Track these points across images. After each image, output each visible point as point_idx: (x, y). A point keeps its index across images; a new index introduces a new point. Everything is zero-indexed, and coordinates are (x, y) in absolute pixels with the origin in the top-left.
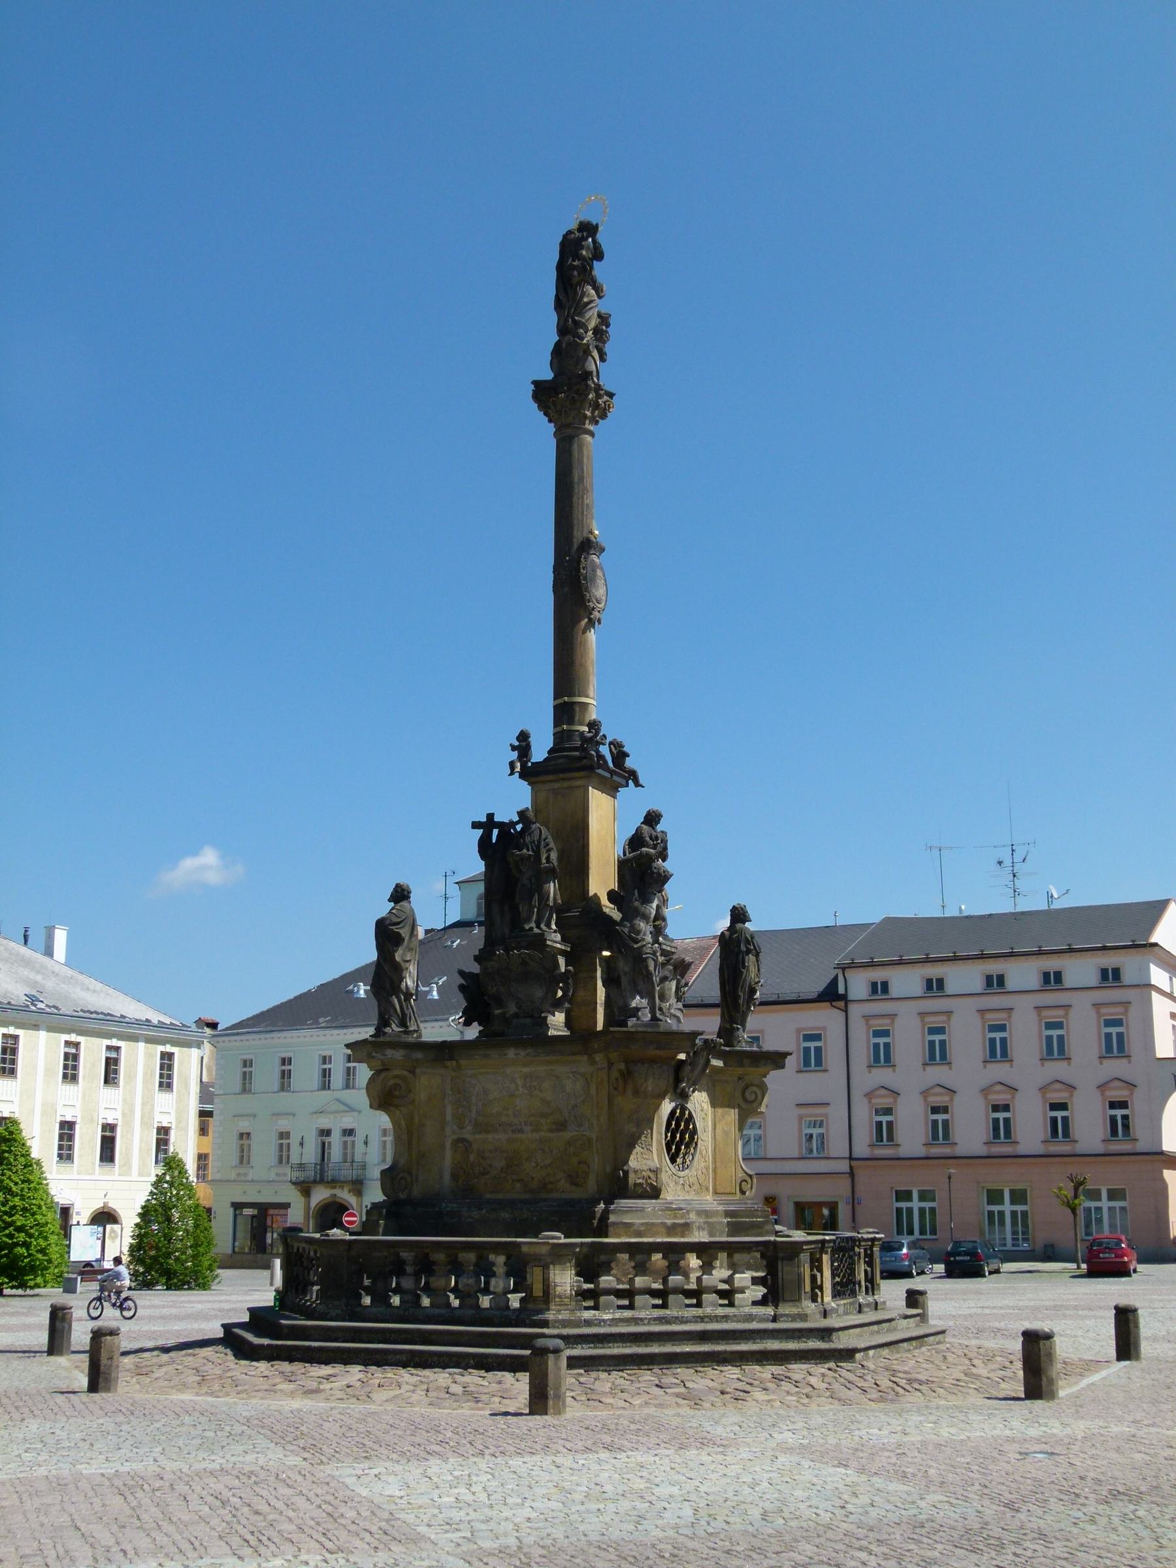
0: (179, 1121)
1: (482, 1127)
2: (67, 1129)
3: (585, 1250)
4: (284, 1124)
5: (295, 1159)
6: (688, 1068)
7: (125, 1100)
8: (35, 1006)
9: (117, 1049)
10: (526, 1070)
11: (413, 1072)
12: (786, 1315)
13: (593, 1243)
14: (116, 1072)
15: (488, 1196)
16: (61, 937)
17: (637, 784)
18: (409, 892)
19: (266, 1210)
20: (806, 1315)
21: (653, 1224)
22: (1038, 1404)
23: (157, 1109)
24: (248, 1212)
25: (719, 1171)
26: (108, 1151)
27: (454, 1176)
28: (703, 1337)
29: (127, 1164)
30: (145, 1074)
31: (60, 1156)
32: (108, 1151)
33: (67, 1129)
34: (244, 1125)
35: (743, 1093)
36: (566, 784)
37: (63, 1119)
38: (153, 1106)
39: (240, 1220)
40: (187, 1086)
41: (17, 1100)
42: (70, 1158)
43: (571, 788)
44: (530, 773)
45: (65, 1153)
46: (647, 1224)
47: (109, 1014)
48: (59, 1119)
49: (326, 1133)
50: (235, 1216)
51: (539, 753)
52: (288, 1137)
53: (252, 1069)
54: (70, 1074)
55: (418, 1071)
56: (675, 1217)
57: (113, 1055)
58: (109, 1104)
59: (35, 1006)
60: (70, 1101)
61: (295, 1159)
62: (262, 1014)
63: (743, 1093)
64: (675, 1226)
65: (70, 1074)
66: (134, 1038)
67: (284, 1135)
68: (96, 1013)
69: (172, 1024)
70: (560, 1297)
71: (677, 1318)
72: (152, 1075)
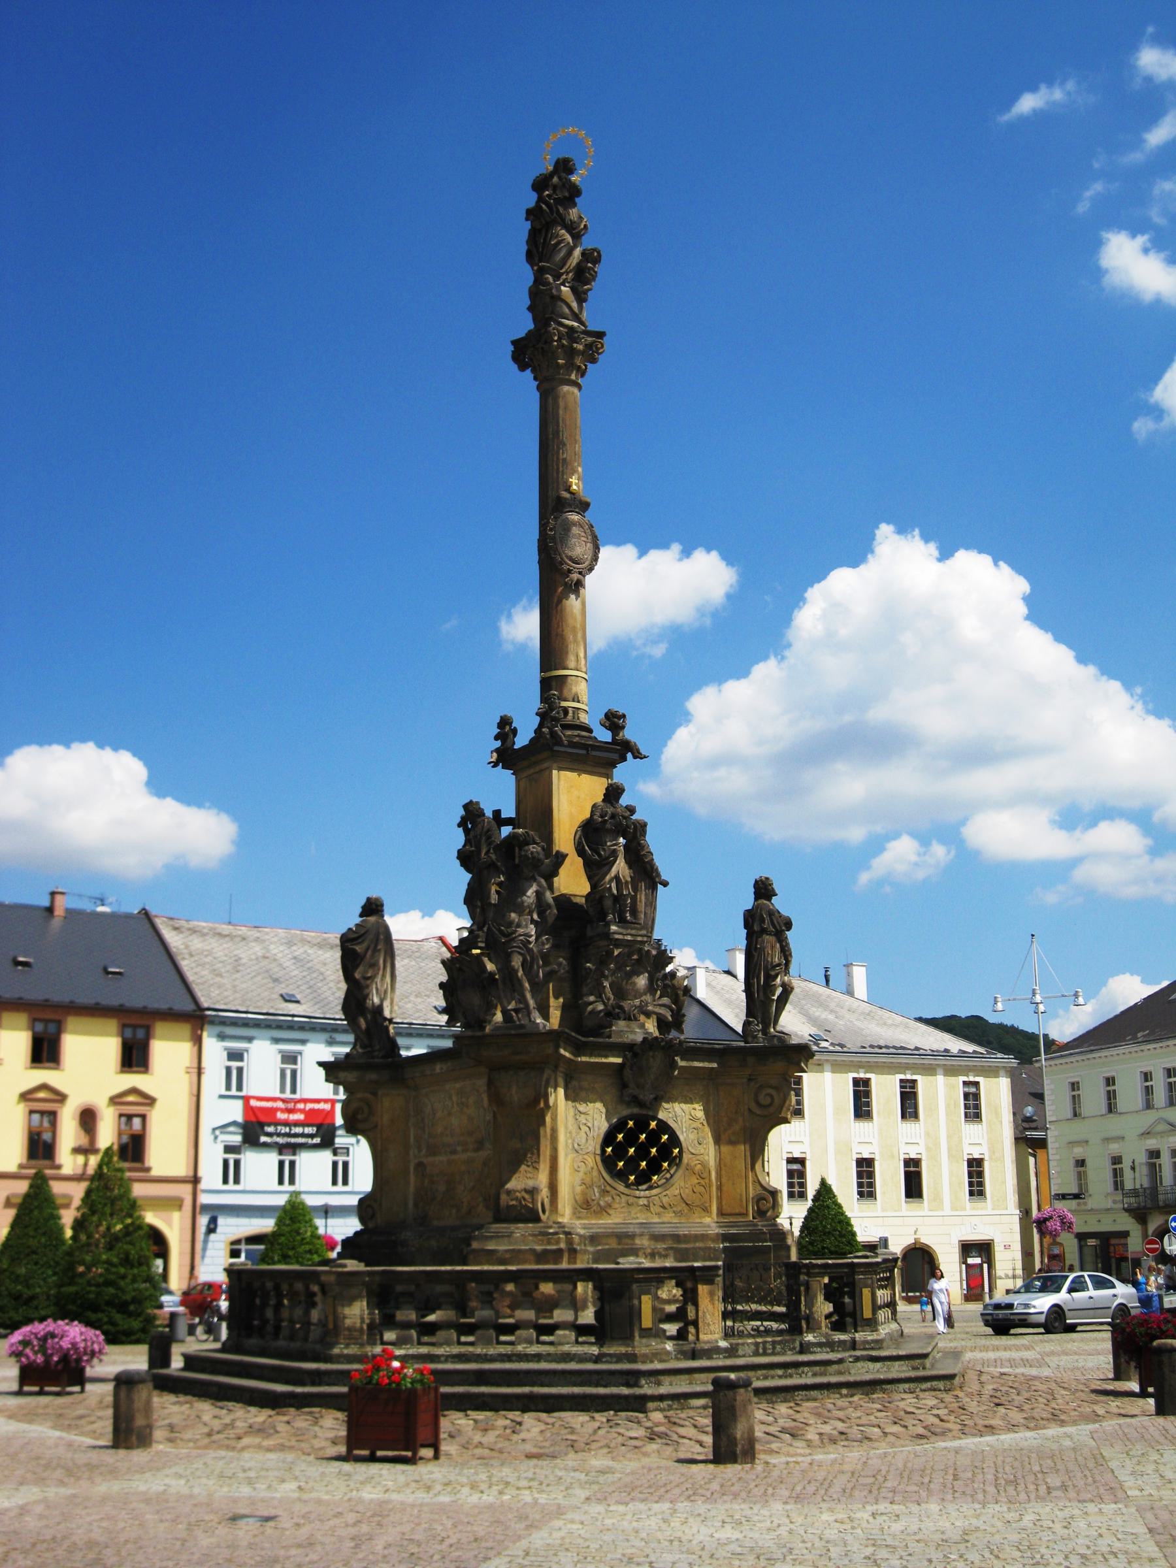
0: (992, 1151)
1: (433, 1151)
2: (865, 1167)
3: (377, 1278)
4: (1115, 1148)
5: (1128, 1185)
6: (627, 1072)
7: (927, 1134)
8: (817, 1045)
9: (976, 1084)
10: (458, 1085)
11: (375, 1094)
12: (610, 1355)
13: (384, 1271)
14: (868, 1104)
15: (435, 1223)
16: (860, 975)
17: (638, 755)
18: (382, 905)
19: (1108, 1239)
20: (635, 1355)
21: (520, 1251)
22: (730, 1471)
23: (966, 1141)
24: (1092, 1242)
25: (724, 1189)
26: (913, 1187)
27: (416, 1205)
28: (481, 1378)
29: (938, 1198)
30: (948, 1106)
31: (861, 1194)
32: (913, 1187)
33: (865, 1167)
34: (1078, 1152)
35: (756, 1095)
36: (537, 769)
37: (859, 1156)
38: (960, 1138)
39: (1086, 1251)
40: (997, 1114)
41: (806, 1140)
42: (981, 1193)
43: (541, 771)
44: (506, 757)
45: (867, 1190)
46: (513, 1250)
47: (902, 1048)
48: (855, 1157)
49: (1155, 1154)
50: (1081, 1248)
51: (522, 740)
52: (1120, 1162)
53: (1080, 1092)
54: (862, 1109)
55: (380, 1093)
56: (549, 1243)
57: (973, 1090)
58: (910, 1139)
59: (817, 1045)
60: (866, 1138)
61: (1128, 1185)
62: (1088, 1033)
63: (756, 1095)
64: (545, 1252)
65: (862, 1109)
66: (930, 1070)
67: (1117, 1160)
68: (887, 1047)
69: (975, 1052)
70: (349, 1329)
71: (479, 1355)
72: (956, 1105)
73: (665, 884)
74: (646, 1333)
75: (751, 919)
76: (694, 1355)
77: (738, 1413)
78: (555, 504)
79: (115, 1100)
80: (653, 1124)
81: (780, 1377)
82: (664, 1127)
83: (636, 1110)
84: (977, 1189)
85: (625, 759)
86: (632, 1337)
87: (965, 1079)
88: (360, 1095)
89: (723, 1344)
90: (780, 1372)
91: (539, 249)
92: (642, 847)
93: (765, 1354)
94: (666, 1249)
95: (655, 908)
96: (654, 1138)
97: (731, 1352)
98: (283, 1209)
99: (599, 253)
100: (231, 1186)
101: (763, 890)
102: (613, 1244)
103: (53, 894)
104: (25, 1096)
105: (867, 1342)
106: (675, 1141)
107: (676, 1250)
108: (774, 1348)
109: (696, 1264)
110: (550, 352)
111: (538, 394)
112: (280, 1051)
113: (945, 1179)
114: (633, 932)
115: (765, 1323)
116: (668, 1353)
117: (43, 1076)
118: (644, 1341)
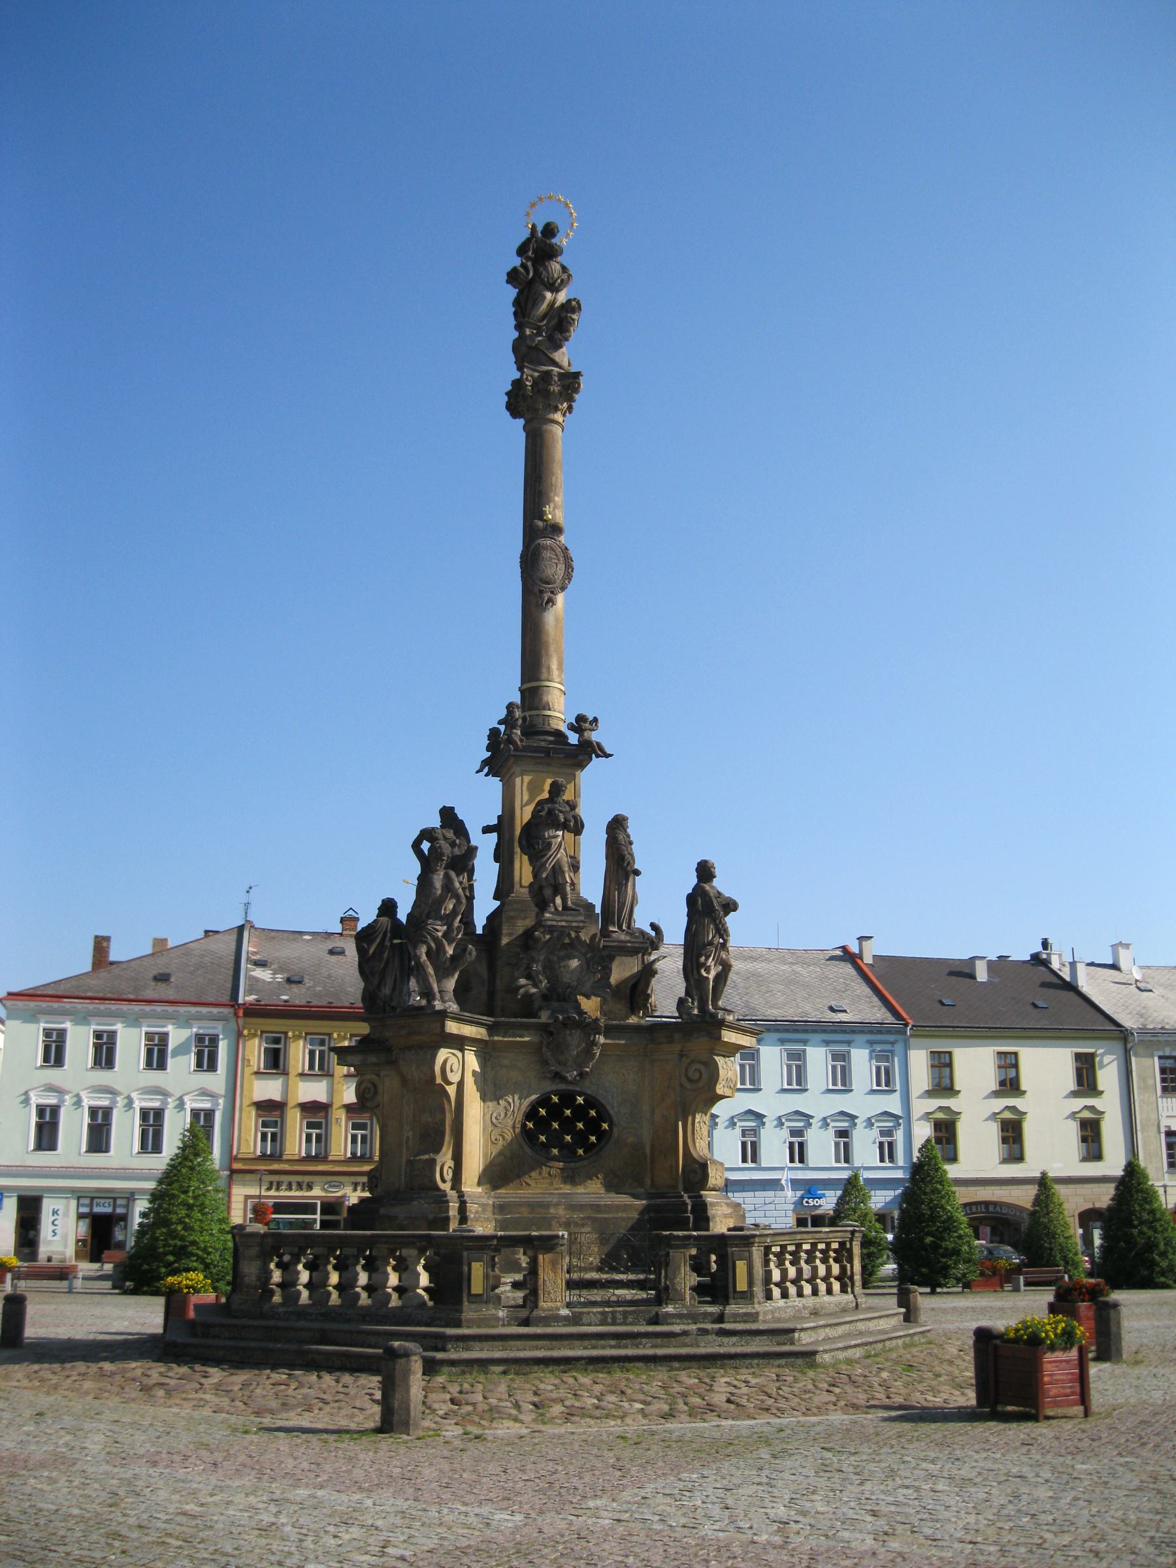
55: (382, 1073)
74: (476, 1299)
75: (691, 900)
76: (526, 1322)
77: (397, 1383)
78: (538, 532)
80: (580, 1100)
81: (612, 1347)
82: (591, 1102)
83: (563, 1086)
85: (591, 759)
86: (460, 1302)
87: (1161, 1054)
88: (368, 1077)
89: (565, 1312)
90: (613, 1342)
91: (523, 308)
93: (614, 1323)
94: (582, 1219)
96: (580, 1113)
97: (575, 1320)
99: (578, 302)
100: (750, 1165)
101: (705, 872)
102: (525, 1213)
103: (1115, 947)
105: (738, 1315)
106: (603, 1115)
107: (594, 1220)
108: (625, 1318)
109: (534, 1233)
110: (539, 395)
111: (524, 435)
112: (786, 1050)
114: (569, 918)
115: (617, 1292)
116: (498, 1319)
118: (473, 1306)
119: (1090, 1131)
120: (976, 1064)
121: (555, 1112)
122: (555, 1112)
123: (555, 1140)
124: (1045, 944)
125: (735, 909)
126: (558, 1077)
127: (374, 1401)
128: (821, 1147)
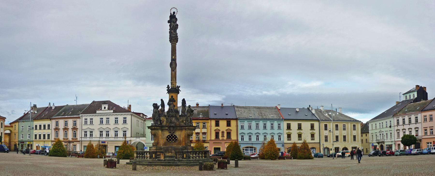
29: (348, 142)
32: (345, 140)
42: (327, 141)
73: (222, 104)
79: (226, 130)
82: (175, 135)
84: (355, 140)
92: (90, 105)
95: (209, 106)
96: (173, 137)
98: (88, 146)
104: (215, 130)
106: (176, 137)
113: (350, 138)
117: (228, 128)
119: (313, 136)
120: (294, 125)
121: (170, 137)
122: (170, 137)
123: (170, 140)
124: (310, 106)
125: (36, 105)
126: (170, 133)
127: (370, 156)
128: (246, 138)
